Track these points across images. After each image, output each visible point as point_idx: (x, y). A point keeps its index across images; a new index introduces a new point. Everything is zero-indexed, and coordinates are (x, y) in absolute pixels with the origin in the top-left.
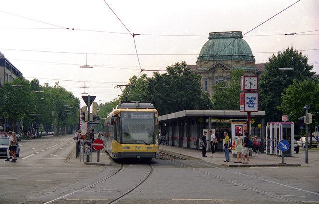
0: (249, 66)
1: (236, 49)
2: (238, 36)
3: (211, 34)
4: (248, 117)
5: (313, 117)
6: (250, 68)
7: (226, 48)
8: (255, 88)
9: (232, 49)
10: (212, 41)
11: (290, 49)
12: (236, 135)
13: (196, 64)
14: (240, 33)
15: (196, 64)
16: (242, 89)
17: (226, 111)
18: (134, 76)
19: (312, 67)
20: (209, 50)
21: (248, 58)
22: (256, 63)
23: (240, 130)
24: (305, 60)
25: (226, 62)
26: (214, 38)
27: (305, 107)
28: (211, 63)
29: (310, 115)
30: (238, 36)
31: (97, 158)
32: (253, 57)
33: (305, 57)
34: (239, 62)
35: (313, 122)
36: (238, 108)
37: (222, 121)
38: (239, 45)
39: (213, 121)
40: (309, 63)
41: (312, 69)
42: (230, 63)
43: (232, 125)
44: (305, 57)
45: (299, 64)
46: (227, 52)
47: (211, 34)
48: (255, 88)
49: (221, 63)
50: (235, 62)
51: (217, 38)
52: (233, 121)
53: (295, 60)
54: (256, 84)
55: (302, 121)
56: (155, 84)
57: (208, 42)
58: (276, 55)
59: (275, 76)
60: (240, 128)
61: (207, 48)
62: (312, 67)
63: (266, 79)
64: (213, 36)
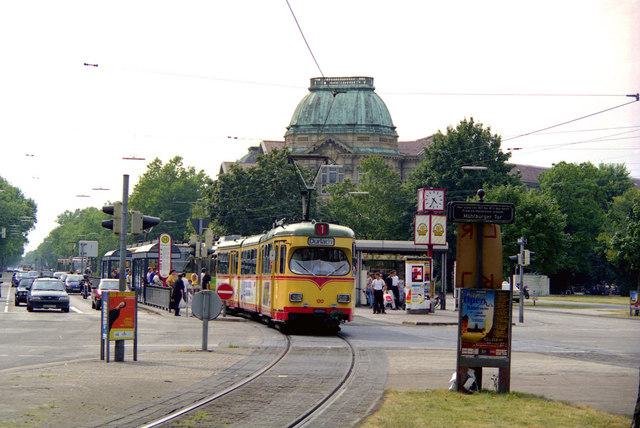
0: (388, 147)
1: (362, 111)
2: (366, 85)
3: (313, 80)
4: (431, 252)
5: (531, 255)
6: (387, 150)
7: (344, 110)
8: (441, 207)
9: (355, 113)
10: (315, 94)
11: (468, 121)
12: (414, 280)
13: (283, 140)
14: (369, 80)
15: (283, 140)
16: (420, 208)
17: (386, 242)
18: (157, 160)
19: (509, 155)
20: (310, 114)
21: (383, 131)
22: (399, 140)
23: (419, 273)
24: (497, 143)
25: (341, 138)
26: (319, 89)
27: (520, 241)
28: (314, 138)
29: (527, 253)
30: (366, 85)
31: (201, 333)
32: (394, 128)
33: (496, 136)
34: (367, 139)
35: (416, 192)
36: (410, 236)
37: (376, 257)
38: (367, 105)
39: (363, 256)
40: (504, 149)
41: (510, 159)
42: (350, 138)
43: (407, 265)
44: (496, 136)
45: (486, 148)
46: (344, 118)
47: (313, 80)
48: (441, 207)
49: (333, 139)
50: (360, 139)
51: (324, 89)
52: (408, 259)
53: (477, 141)
54: (442, 202)
55: (516, 261)
56: (232, 186)
57: (308, 98)
58: (444, 133)
59: (443, 171)
60: (419, 269)
61: (307, 109)
62: (509, 155)
63: (427, 176)
64: (317, 85)
